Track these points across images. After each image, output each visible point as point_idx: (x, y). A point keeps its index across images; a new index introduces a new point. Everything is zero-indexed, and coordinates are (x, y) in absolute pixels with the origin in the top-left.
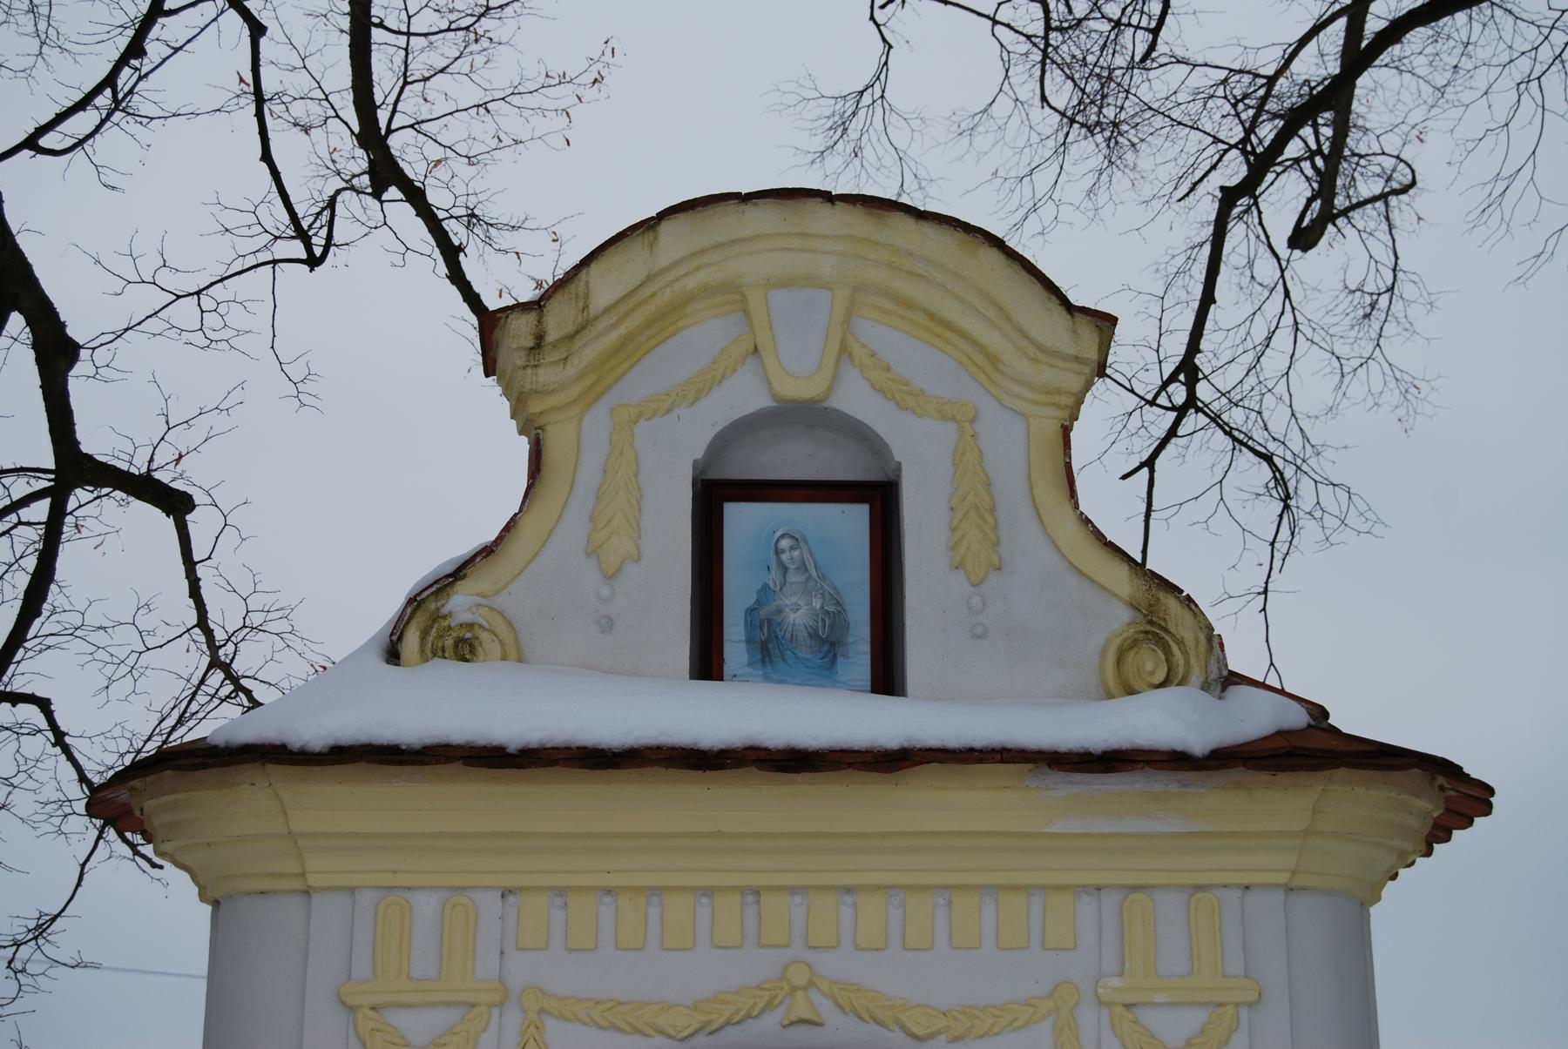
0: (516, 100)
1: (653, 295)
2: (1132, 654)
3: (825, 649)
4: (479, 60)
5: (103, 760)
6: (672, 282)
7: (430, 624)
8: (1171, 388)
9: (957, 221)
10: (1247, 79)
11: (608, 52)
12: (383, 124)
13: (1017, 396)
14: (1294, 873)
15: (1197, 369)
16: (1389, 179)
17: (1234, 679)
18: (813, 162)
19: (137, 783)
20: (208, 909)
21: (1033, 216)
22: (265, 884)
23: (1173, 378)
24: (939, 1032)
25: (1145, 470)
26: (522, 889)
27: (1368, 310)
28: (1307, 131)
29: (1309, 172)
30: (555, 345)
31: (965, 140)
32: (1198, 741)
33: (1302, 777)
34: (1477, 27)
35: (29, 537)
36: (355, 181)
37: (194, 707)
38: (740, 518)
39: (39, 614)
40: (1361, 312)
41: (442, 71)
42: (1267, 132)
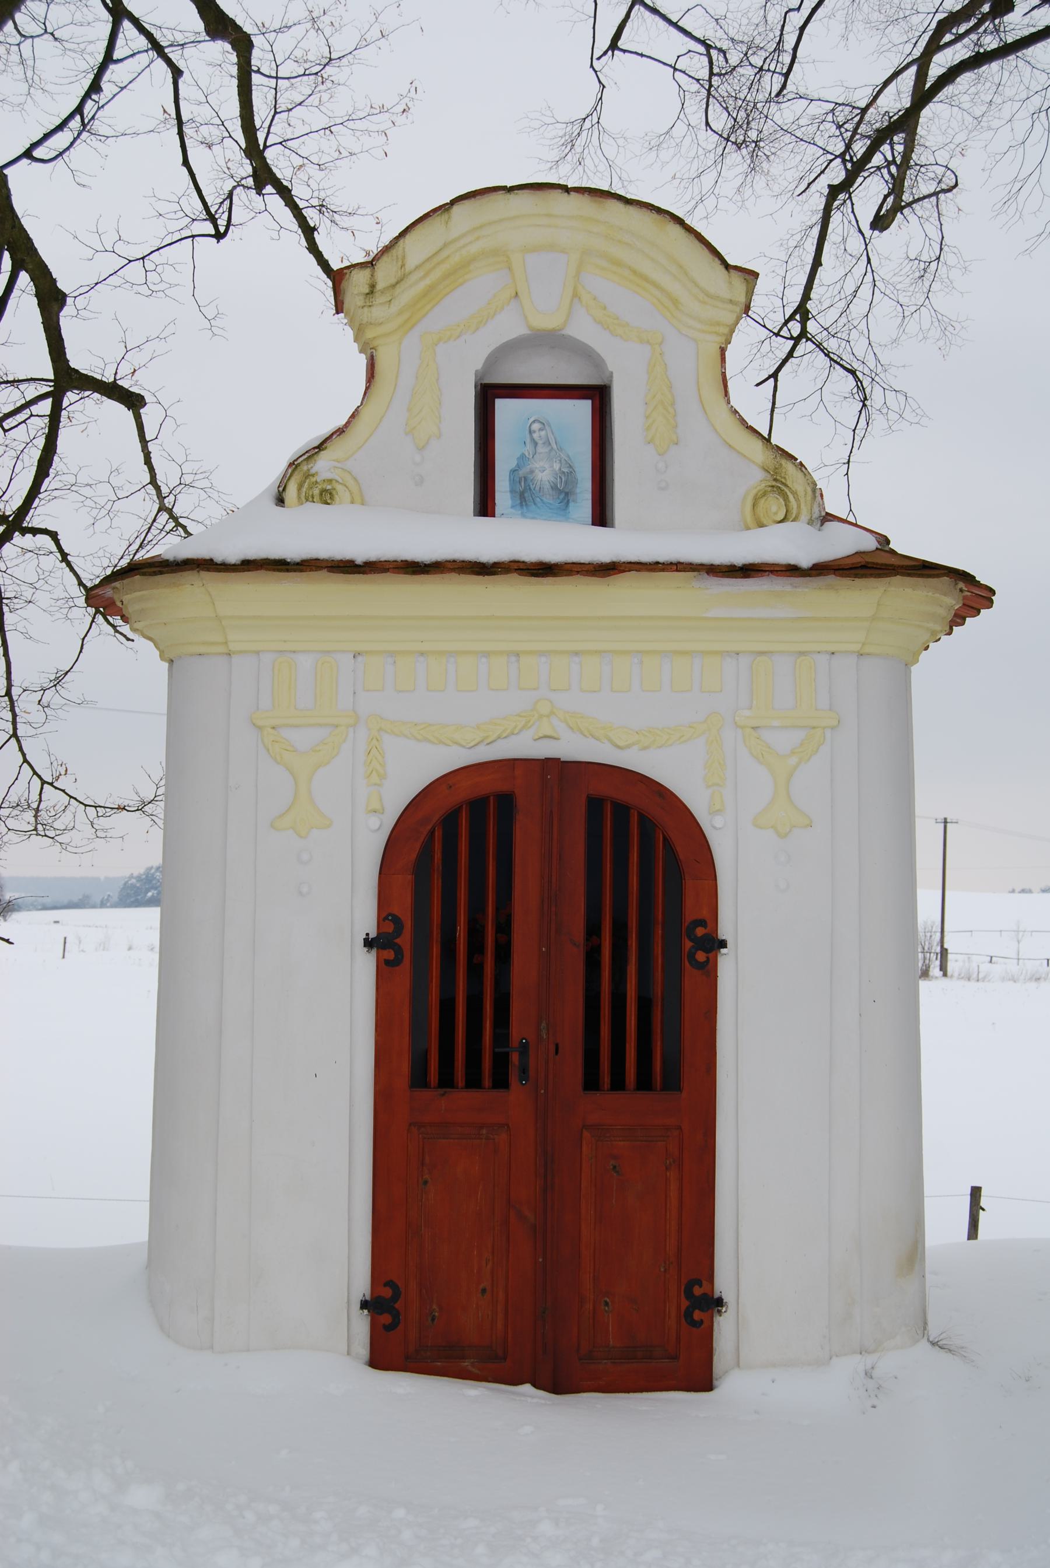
0: (350, 124)
1: (448, 257)
2: (763, 501)
3: (562, 496)
4: (325, 96)
5: (93, 572)
6: (464, 246)
7: (302, 479)
8: (790, 325)
9: (653, 206)
10: (848, 109)
11: (413, 90)
12: (261, 142)
14: (863, 644)
15: (808, 312)
16: (939, 182)
17: (828, 517)
18: (551, 168)
19: (117, 584)
20: (166, 665)
21: (700, 206)
22: (202, 649)
23: (792, 318)
24: (634, 744)
25: (772, 380)
26: (367, 652)
27: (922, 272)
28: (886, 148)
29: (887, 177)
30: (382, 292)
31: (654, 153)
33: (872, 582)
34: (1006, 74)
35: (39, 425)
36: (243, 182)
37: (150, 537)
38: (505, 409)
39: (48, 475)
40: (917, 274)
41: (300, 104)
42: (859, 148)
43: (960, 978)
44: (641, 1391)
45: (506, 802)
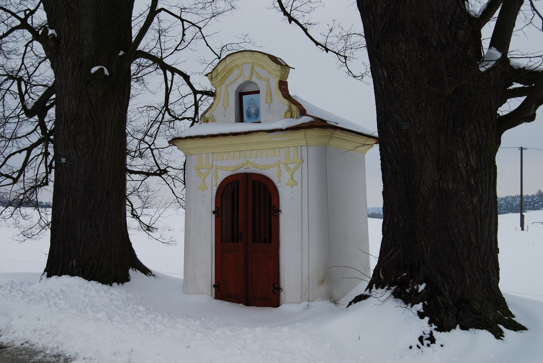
32: (284, 127)
33: (301, 130)
38: (245, 98)
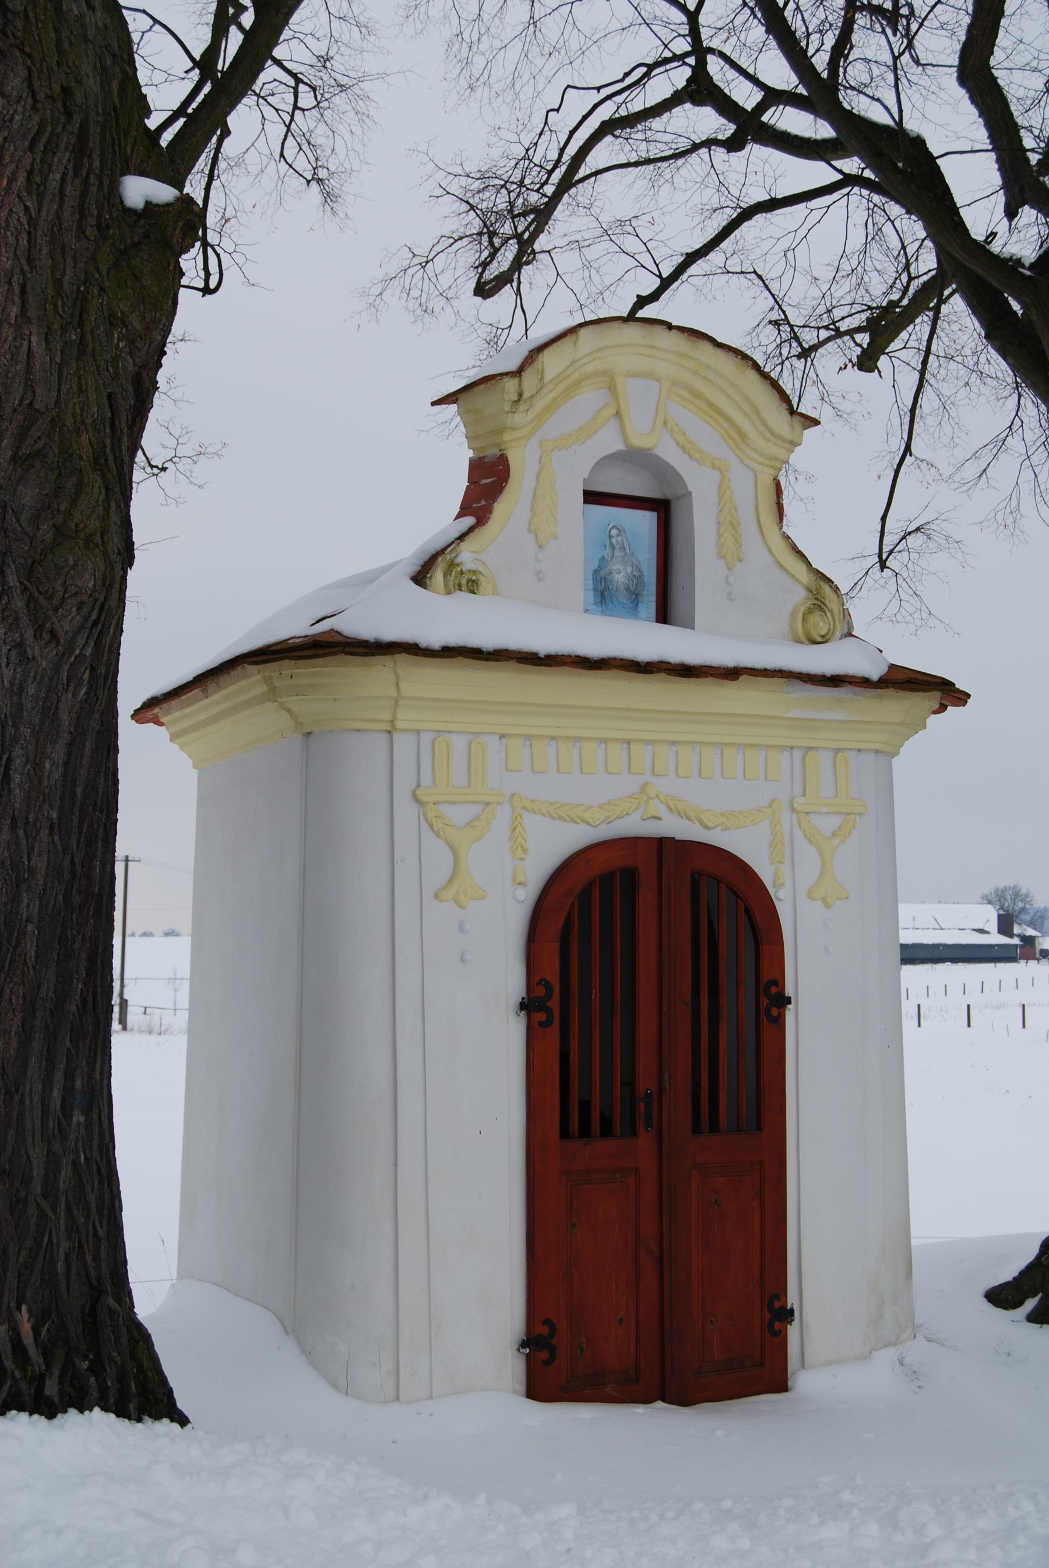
13: (753, 459)
43: (141, 1032)
44: (740, 1397)
45: (630, 876)
